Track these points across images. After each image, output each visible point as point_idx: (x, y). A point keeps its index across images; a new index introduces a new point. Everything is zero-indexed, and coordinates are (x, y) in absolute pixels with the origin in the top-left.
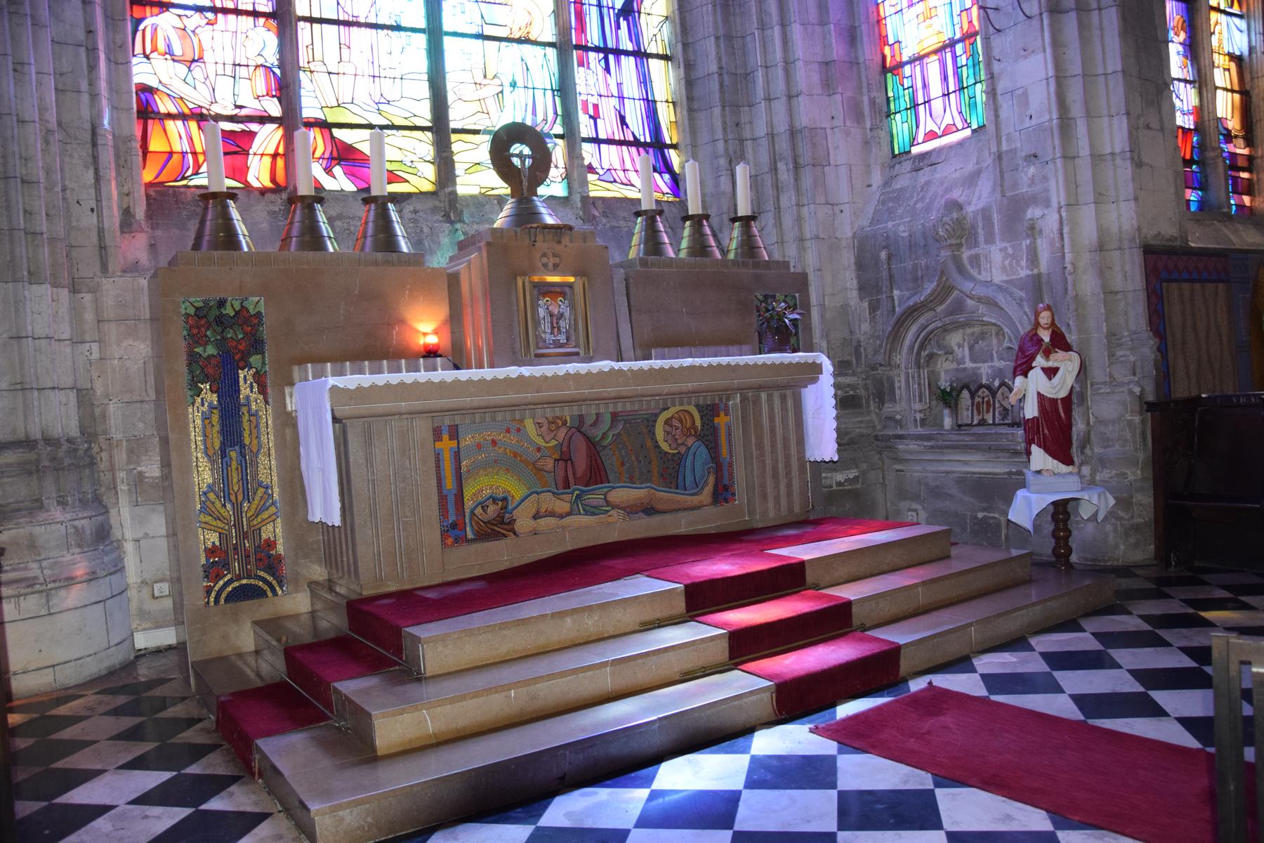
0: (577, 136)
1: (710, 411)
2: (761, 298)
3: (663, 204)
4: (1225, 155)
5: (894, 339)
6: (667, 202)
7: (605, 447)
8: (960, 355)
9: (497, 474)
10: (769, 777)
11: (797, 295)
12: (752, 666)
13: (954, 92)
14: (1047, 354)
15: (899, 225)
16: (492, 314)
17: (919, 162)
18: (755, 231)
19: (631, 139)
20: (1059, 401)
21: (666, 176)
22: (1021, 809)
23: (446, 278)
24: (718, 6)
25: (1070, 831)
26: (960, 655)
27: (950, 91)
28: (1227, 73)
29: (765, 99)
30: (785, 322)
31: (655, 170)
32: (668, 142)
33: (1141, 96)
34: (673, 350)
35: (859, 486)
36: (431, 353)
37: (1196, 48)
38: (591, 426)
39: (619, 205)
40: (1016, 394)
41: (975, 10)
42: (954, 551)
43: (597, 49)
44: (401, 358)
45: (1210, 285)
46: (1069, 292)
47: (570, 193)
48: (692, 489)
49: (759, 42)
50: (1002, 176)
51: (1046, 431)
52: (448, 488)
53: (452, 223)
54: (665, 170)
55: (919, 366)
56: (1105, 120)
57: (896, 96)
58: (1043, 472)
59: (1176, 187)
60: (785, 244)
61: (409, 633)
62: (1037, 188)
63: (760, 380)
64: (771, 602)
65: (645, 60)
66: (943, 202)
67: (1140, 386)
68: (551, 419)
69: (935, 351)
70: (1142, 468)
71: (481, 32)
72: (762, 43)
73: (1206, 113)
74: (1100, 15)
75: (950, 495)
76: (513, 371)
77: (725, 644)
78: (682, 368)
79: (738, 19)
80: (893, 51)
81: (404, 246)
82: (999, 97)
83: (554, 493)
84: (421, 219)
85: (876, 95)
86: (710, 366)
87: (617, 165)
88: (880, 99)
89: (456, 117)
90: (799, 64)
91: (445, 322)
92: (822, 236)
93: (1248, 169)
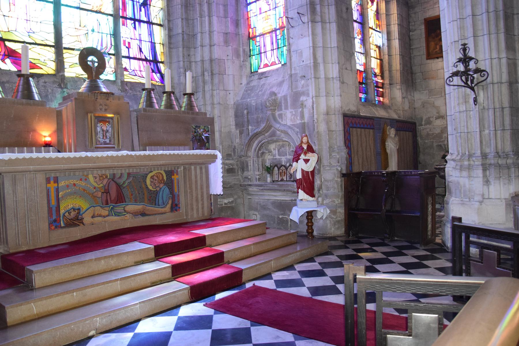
0: (120, 55)
1: (170, 173)
2: (194, 127)
3: (156, 86)
4: (374, 82)
5: (248, 146)
6: (158, 85)
7: (124, 187)
8: (274, 153)
9: (75, 198)
10: (185, 325)
11: (209, 127)
12: (181, 279)
13: (276, 49)
14: (305, 154)
15: (252, 100)
16: (76, 129)
17: (261, 76)
18: (193, 99)
19: (144, 58)
20: (310, 172)
21: (158, 75)
22: (283, 333)
23: (55, 112)
24: (183, 6)
25: (301, 341)
26: (267, 273)
27: (274, 49)
28: (375, 52)
29: (201, 46)
30: (202, 137)
31: (153, 71)
32: (160, 60)
33: (344, 57)
34: (156, 147)
35: (233, 205)
36: (47, 145)
37: (364, 41)
38: (118, 178)
39: (137, 85)
40: (293, 169)
41: (284, 17)
42: (268, 231)
43: (131, 19)
44: (33, 147)
45: (367, 130)
46: (315, 130)
47: (116, 79)
48: (162, 205)
49: (200, 22)
50: (292, 83)
51: (304, 184)
52: (53, 204)
53: (62, 88)
54: (157, 72)
55: (258, 157)
56: (330, 65)
57: (253, 49)
58: (303, 200)
59: (356, 92)
60: (206, 106)
61: (28, 269)
62: (304, 89)
63: (191, 161)
64: (191, 252)
65: (151, 26)
66: (269, 92)
67: (341, 167)
68: (100, 175)
69: (265, 151)
70: (341, 199)
71: (79, 6)
72: (200, 23)
73: (368, 66)
74: (330, 25)
75: (269, 209)
76: (83, 154)
77: (170, 270)
78: (158, 155)
79: (191, 12)
80: (253, 31)
81: (37, 97)
82: (292, 52)
83: (101, 207)
84: (48, 86)
85: (245, 47)
86: (170, 154)
87: (137, 69)
88: (247, 50)
89: (66, 42)
90: (215, 33)
91: (54, 132)
92: (221, 103)
93: (382, 88)
